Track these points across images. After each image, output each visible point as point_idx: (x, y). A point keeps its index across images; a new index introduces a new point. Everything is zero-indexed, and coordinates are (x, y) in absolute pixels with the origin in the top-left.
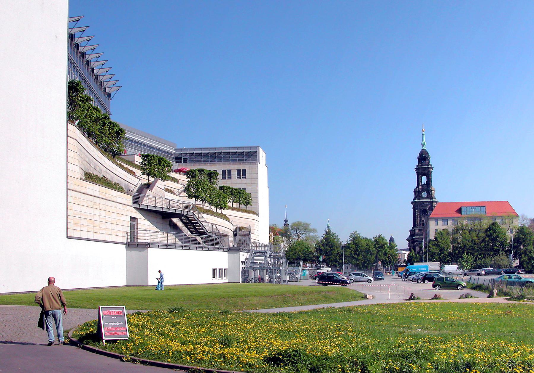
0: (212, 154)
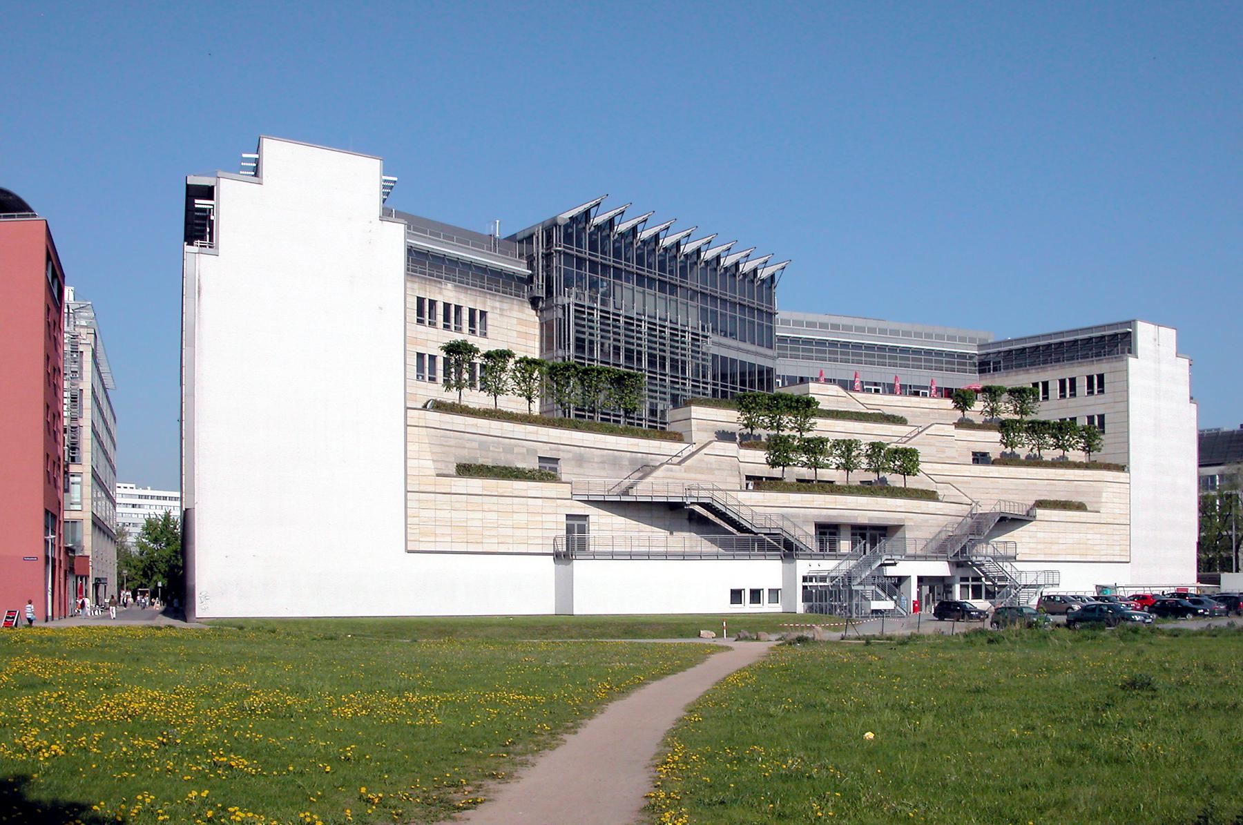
0: (1057, 346)
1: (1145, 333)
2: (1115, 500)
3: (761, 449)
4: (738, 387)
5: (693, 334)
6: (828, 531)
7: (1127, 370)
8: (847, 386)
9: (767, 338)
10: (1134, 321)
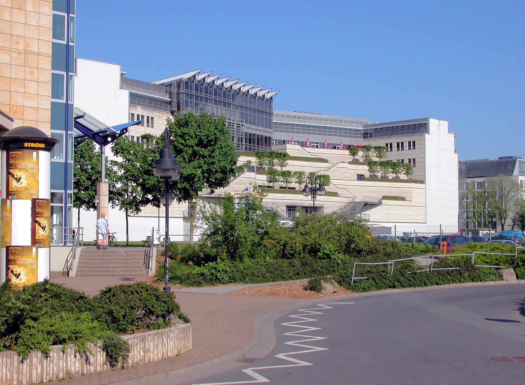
1: (433, 123)
2: (419, 196)
3: (265, 174)
4: (256, 145)
5: (237, 124)
6: (292, 209)
7: (425, 140)
8: (303, 144)
9: (269, 124)
10: (428, 118)
